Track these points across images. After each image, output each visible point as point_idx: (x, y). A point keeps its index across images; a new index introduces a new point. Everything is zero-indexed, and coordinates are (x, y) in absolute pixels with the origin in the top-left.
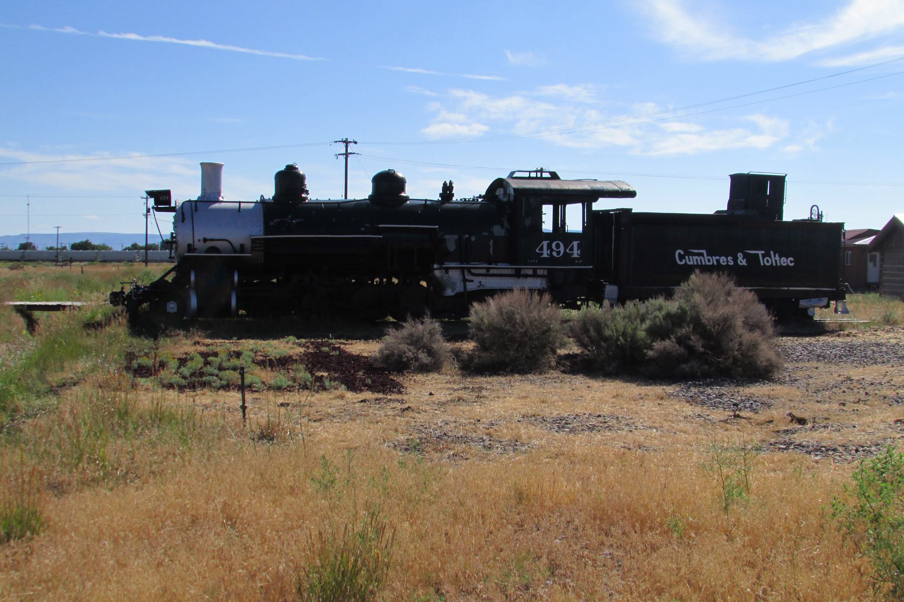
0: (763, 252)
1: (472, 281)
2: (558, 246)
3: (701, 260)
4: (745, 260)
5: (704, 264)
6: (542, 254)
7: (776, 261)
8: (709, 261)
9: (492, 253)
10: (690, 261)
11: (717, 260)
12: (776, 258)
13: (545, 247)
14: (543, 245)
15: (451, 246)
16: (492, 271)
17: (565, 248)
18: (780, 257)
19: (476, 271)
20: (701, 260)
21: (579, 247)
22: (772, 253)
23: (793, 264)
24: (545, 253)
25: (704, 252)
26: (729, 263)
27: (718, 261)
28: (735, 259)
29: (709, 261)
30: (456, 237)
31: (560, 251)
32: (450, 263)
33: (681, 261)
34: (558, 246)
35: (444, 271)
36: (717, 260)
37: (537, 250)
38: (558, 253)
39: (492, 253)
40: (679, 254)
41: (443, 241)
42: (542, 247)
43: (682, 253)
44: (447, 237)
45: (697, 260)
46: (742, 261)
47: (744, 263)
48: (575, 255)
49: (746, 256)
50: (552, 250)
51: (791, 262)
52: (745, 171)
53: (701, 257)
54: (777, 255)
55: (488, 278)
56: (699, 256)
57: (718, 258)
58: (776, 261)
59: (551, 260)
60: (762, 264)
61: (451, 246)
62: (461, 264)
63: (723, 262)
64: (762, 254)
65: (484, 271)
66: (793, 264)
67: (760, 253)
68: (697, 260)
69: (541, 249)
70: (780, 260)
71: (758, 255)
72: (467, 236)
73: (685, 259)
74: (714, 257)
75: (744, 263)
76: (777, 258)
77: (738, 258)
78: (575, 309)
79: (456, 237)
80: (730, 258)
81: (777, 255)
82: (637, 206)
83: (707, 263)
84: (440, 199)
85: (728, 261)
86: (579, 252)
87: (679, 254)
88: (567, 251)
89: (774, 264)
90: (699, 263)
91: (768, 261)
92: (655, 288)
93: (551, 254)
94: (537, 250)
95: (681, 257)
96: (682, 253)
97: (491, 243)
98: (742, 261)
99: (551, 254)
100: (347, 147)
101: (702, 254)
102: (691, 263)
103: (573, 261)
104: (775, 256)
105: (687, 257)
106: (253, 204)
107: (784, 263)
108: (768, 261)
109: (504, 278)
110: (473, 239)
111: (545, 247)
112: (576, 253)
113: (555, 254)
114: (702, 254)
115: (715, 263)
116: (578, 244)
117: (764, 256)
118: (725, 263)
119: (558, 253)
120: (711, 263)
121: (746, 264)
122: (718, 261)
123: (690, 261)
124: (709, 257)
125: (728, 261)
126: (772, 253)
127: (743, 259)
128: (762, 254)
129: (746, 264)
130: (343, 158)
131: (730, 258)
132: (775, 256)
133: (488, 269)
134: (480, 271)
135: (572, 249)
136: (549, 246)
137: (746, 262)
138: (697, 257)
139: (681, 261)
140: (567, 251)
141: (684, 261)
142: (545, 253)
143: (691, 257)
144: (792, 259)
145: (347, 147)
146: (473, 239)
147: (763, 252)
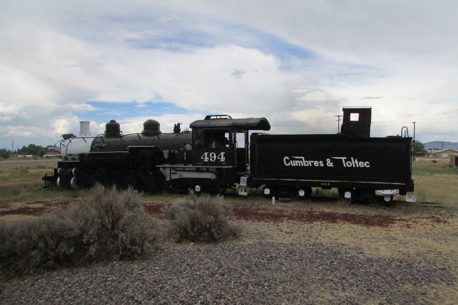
0: (346, 158)
1: (177, 174)
2: (213, 155)
3: (301, 163)
4: (332, 163)
5: (302, 165)
6: (204, 160)
7: (355, 164)
8: (306, 163)
9: (185, 159)
10: (293, 164)
11: (312, 163)
12: (355, 162)
13: (206, 156)
14: (205, 155)
15: (166, 156)
16: (186, 169)
17: (217, 156)
18: (359, 161)
19: (179, 169)
20: (301, 163)
21: (225, 156)
22: (352, 158)
23: (369, 166)
24: (206, 159)
25: (303, 158)
26: (320, 165)
27: (312, 164)
28: (325, 163)
29: (306, 163)
30: (168, 151)
31: (214, 158)
32: (166, 164)
33: (287, 163)
34: (213, 155)
35: (163, 168)
36: (312, 163)
37: (202, 158)
38: (213, 159)
39: (185, 159)
40: (286, 159)
41: (162, 154)
42: (204, 156)
43: (288, 158)
44: (164, 151)
45: (298, 163)
46: (330, 164)
47: (331, 165)
48: (222, 160)
49: (332, 160)
50: (210, 158)
51: (367, 164)
52: (372, 111)
53: (301, 161)
54: (356, 160)
55: (184, 172)
56: (299, 161)
57: (312, 162)
58: (355, 164)
59: (209, 163)
60: (345, 166)
61: (166, 156)
62: (171, 165)
63: (316, 164)
64: (345, 159)
65: (182, 169)
66: (369, 166)
67: (343, 159)
68: (298, 163)
69: (204, 157)
70: (358, 164)
71: (342, 159)
72: (173, 150)
73: (290, 162)
74: (309, 161)
75: (331, 165)
76: (356, 162)
77: (327, 162)
78: (34, 208)
79: (168, 151)
80: (321, 162)
81: (356, 160)
82: (273, 131)
83: (305, 165)
84: (174, 132)
85: (319, 164)
86: (224, 159)
87: (286, 159)
88: (218, 158)
89: (354, 166)
90: (300, 165)
91: (349, 164)
92: (272, 179)
93: (209, 160)
94: (202, 158)
95: (288, 161)
96: (288, 158)
97: (185, 154)
98: (330, 164)
99: (209, 160)
100: (339, 118)
101: (301, 160)
102: (294, 165)
103: (221, 164)
104: (354, 161)
105: (291, 161)
106: (94, 138)
107: (362, 165)
108: (349, 164)
109: (190, 172)
110: (176, 152)
111: (206, 156)
112: (223, 159)
113: (211, 160)
114: (301, 160)
115: (311, 165)
116: (224, 154)
117: (346, 161)
118: (318, 165)
119: (213, 159)
120: (308, 165)
121: (332, 166)
122: (312, 164)
123: (293, 164)
124: (307, 162)
125: (319, 164)
126: (352, 158)
127: (331, 162)
128: (345, 159)
129: (332, 166)
130: (338, 121)
131: (321, 162)
132: (354, 161)
133: (184, 168)
134: (180, 169)
135: (220, 157)
136: (208, 156)
137: (333, 165)
138: (298, 161)
139: (287, 163)
140: (218, 158)
141: (289, 164)
142: (206, 159)
143: (294, 161)
144: (368, 163)
145: (339, 118)
146: (176, 152)
147: (346, 158)
